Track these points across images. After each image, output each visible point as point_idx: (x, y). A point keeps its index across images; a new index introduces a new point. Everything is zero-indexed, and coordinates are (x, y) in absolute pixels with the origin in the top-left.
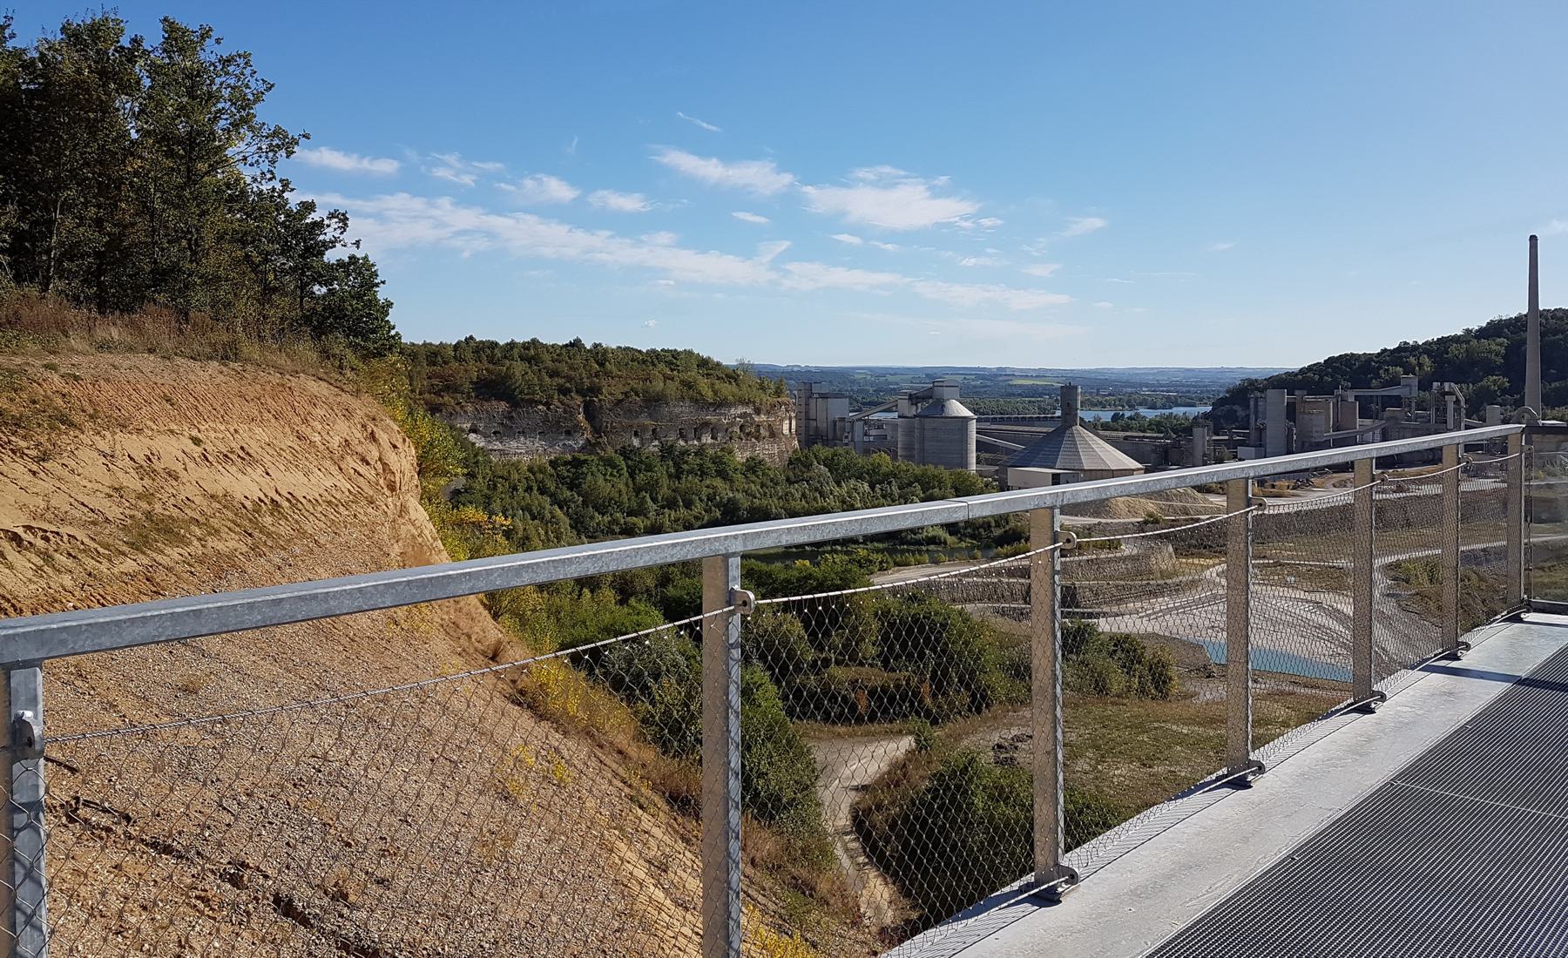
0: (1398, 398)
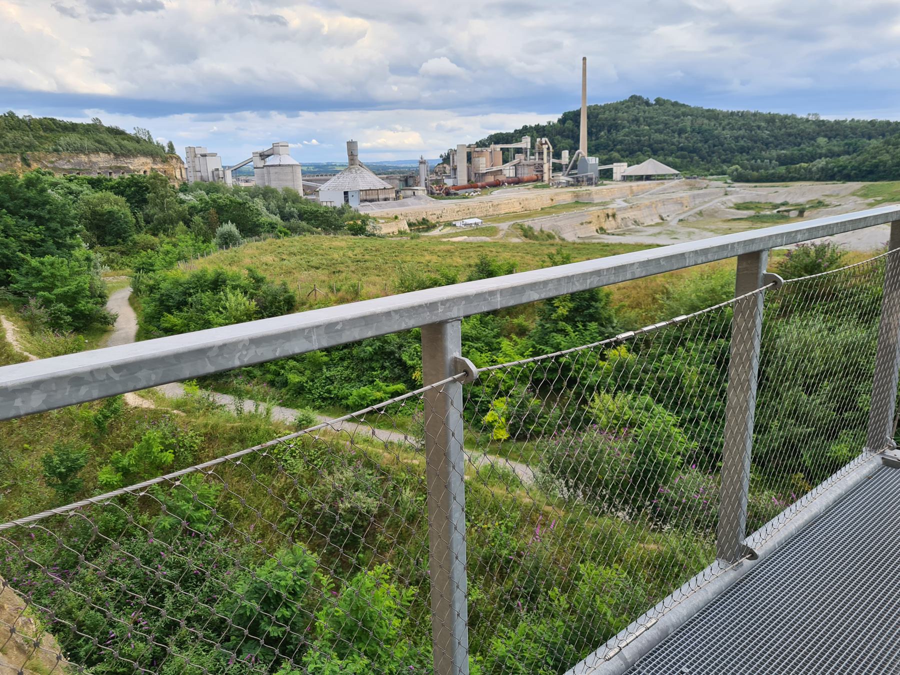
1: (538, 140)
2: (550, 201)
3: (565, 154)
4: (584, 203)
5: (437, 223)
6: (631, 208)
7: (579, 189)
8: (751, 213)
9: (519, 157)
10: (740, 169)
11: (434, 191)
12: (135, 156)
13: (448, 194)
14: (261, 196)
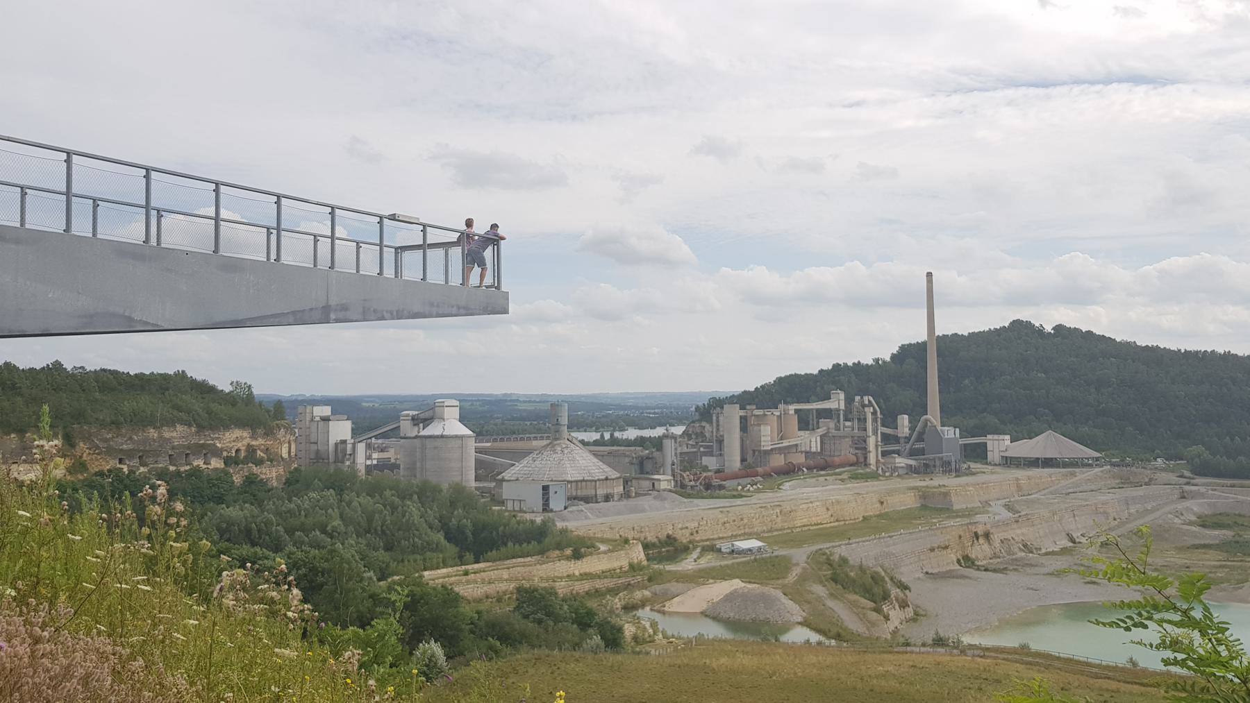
0: (830, 410)
1: (857, 398)
2: (878, 505)
3: (904, 420)
4: (936, 509)
5: (690, 542)
6: (1017, 521)
7: (927, 483)
8: (1227, 534)
9: (827, 425)
10: (1206, 455)
11: (686, 482)
12: (227, 428)
13: (710, 489)
14: (415, 497)
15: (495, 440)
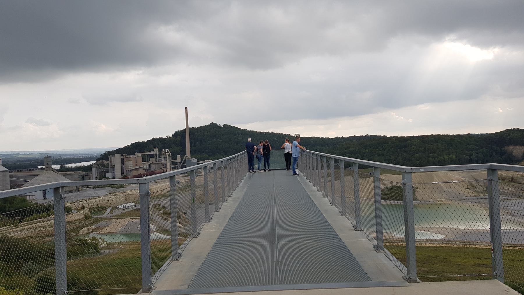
3: (179, 157)
9: (153, 160)
15: (15, 171)
